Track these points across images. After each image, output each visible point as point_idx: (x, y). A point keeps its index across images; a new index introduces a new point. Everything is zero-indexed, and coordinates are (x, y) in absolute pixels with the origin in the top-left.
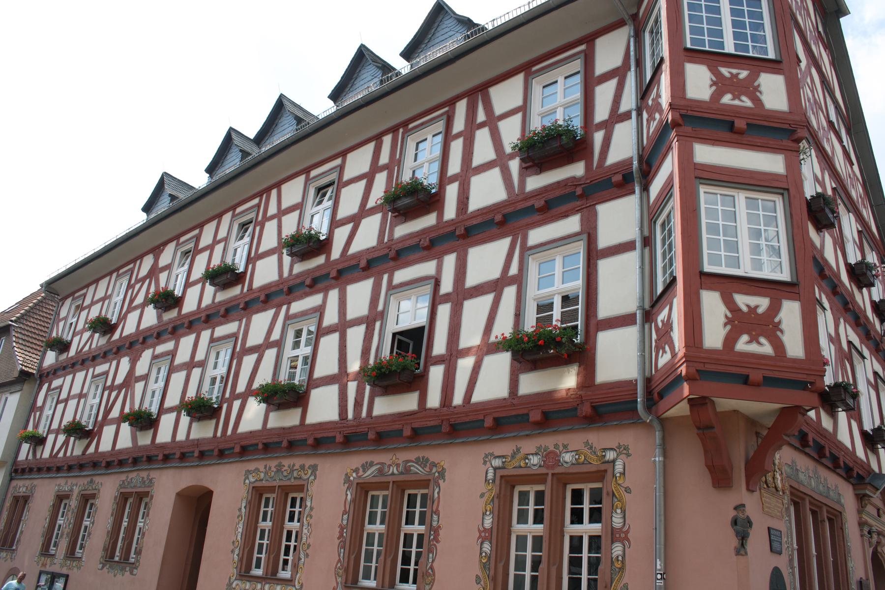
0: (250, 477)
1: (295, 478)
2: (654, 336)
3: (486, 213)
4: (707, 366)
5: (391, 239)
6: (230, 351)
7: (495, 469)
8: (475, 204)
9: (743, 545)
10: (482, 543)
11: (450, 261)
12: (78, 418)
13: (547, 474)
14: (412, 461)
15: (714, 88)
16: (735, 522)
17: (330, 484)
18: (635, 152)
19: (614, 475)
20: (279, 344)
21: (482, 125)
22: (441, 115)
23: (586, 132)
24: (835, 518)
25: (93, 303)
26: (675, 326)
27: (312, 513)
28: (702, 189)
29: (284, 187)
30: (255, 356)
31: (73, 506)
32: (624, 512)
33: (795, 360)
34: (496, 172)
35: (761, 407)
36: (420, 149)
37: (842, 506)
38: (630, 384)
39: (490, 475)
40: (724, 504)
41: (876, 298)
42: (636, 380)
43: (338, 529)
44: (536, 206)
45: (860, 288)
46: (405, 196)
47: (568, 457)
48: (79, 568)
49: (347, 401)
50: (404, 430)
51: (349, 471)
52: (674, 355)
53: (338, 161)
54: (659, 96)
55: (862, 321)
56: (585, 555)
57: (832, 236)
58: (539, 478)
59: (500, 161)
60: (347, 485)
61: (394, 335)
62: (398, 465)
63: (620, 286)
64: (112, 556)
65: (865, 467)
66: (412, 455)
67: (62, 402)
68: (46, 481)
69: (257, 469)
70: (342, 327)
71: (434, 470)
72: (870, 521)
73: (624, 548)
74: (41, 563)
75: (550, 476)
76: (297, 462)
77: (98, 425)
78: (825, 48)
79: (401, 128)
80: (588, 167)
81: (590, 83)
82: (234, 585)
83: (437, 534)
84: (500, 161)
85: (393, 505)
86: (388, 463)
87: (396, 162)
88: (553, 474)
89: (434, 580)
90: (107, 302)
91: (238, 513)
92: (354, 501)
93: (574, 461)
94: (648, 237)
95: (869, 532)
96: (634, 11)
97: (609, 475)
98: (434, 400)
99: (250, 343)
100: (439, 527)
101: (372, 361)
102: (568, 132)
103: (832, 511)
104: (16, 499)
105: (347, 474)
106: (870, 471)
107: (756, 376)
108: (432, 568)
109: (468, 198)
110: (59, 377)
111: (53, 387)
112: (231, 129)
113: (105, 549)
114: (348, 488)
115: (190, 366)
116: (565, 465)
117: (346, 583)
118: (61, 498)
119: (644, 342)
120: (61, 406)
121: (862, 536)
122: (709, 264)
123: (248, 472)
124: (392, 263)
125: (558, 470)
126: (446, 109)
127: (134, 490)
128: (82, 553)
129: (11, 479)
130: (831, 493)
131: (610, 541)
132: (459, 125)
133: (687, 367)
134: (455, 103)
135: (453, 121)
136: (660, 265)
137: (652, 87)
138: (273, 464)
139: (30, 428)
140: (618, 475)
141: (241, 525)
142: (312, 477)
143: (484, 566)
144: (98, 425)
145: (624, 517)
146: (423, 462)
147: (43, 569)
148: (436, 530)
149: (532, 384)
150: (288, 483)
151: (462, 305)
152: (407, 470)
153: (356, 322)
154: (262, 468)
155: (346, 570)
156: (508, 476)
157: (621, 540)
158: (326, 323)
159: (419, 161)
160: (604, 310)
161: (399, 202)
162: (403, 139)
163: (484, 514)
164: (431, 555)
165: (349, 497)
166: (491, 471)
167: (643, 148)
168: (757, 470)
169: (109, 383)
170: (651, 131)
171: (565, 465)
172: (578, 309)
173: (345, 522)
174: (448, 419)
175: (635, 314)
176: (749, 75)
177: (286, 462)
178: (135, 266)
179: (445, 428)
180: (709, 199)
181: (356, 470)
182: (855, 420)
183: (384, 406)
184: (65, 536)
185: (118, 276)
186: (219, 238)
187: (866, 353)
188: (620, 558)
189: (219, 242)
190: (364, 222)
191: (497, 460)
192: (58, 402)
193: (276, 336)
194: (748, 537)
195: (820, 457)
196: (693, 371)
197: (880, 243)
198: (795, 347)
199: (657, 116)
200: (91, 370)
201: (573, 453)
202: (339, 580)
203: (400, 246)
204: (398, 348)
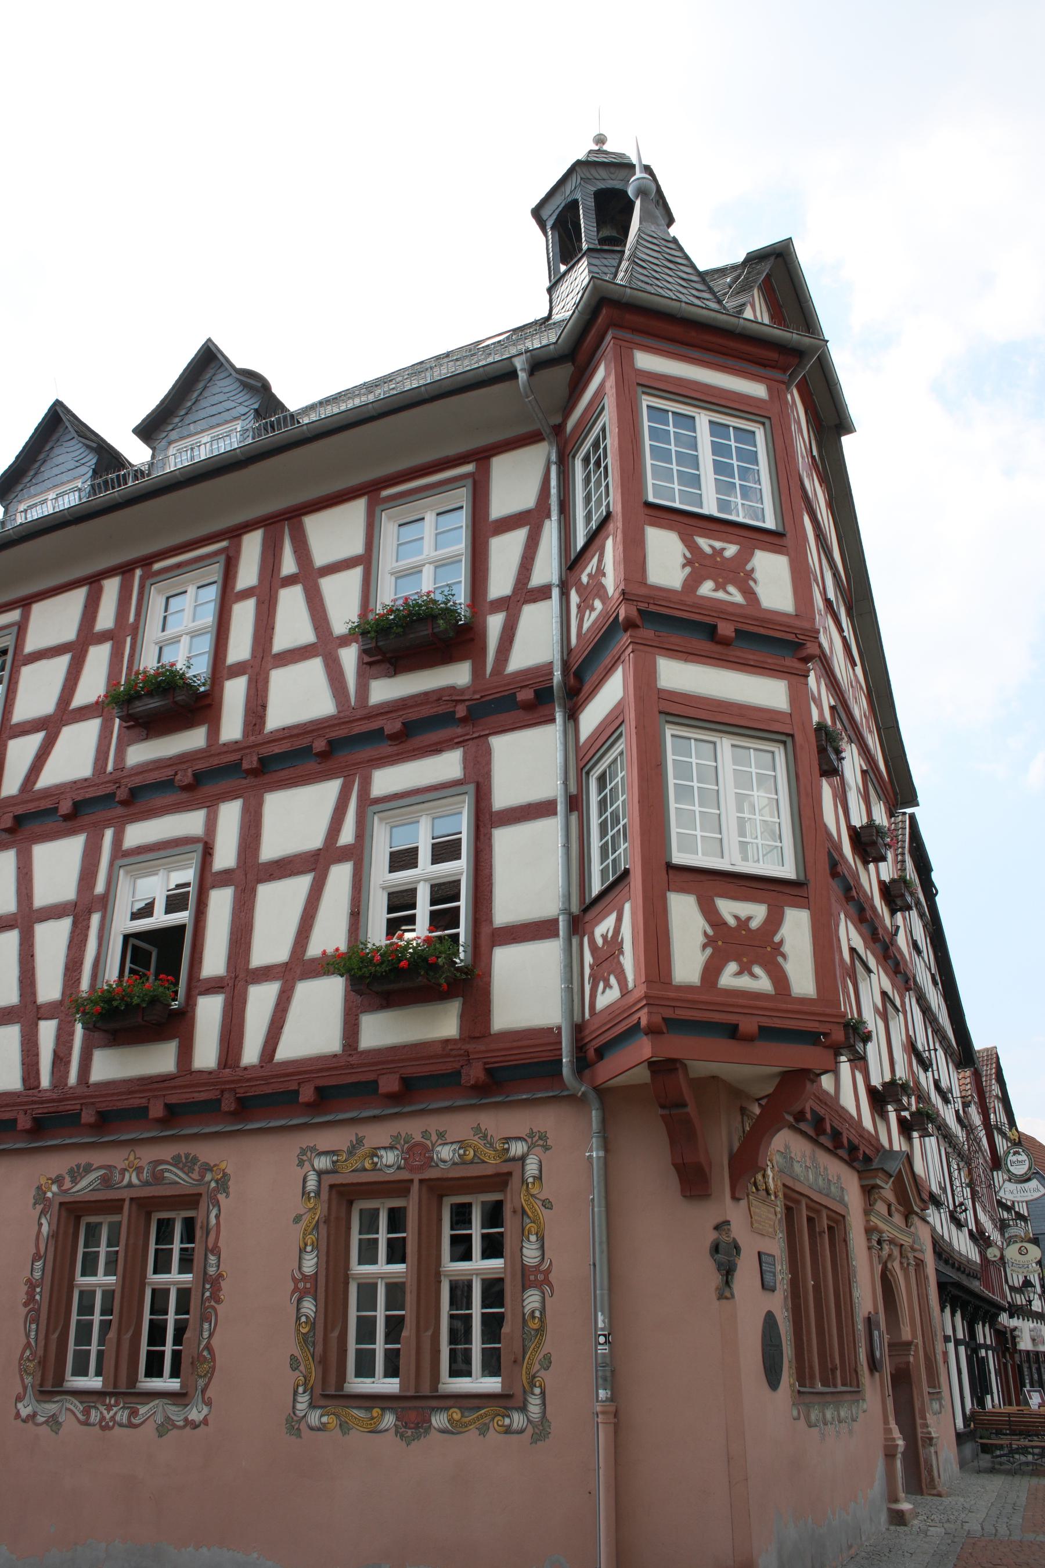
2: (588, 958)
3: (297, 735)
4: (678, 1012)
5: (120, 766)
7: (320, 1174)
8: (276, 719)
9: (728, 1283)
10: (300, 1301)
11: (230, 813)
13: (412, 1181)
14: (168, 1163)
15: (688, 570)
16: (716, 1248)
19: (524, 1181)
21: (290, 581)
23: (474, 614)
24: (838, 1222)
26: (628, 947)
28: (669, 731)
32: (541, 1239)
33: (803, 1001)
34: (315, 666)
35: (753, 1069)
36: (171, 610)
37: (846, 1206)
38: (548, 1036)
39: (312, 1184)
40: (700, 1220)
41: (885, 877)
42: (559, 1028)
45: (866, 863)
46: (150, 694)
49: (37, 1055)
50: (151, 1106)
51: (43, 1181)
52: (625, 992)
53: (15, 615)
54: (600, 572)
55: (869, 913)
56: (477, 1311)
57: (831, 785)
58: (401, 1188)
59: (324, 646)
60: (39, 1208)
61: (127, 938)
62: (139, 1170)
63: (529, 873)
65: (874, 1142)
66: (166, 1152)
71: (208, 1177)
72: (881, 1225)
73: (544, 1298)
75: (416, 1184)
78: (822, 481)
79: (140, 569)
80: (477, 671)
81: (482, 531)
84: (324, 646)
87: (126, 633)
88: (421, 1181)
92: (54, 1235)
93: (457, 1159)
94: (576, 796)
95: (879, 1242)
96: (557, 420)
97: (516, 1179)
98: (206, 1054)
100: (220, 1276)
101: (85, 985)
102: (449, 612)
103: (834, 1215)
105: (39, 1188)
106: (879, 1148)
107: (748, 1025)
108: (208, 1347)
109: (264, 707)
114: (43, 1213)
117: (41, 1385)
121: (870, 1248)
122: (679, 851)
124: (120, 810)
125: (431, 1174)
126: (224, 544)
130: (833, 1189)
131: (520, 1287)
132: (248, 575)
133: (650, 1013)
134: (240, 535)
135: (236, 566)
136: (595, 844)
137: (588, 555)
140: (530, 1180)
143: (305, 1340)
146: (187, 1164)
148: (216, 1282)
149: (380, 1031)
151: (253, 892)
152: (158, 1178)
153: (53, 912)
155: (43, 1363)
157: (538, 1285)
159: (170, 631)
160: (503, 914)
161: (138, 703)
162: (142, 587)
163: (302, 1251)
164: (206, 1326)
165: (45, 1229)
166: (312, 1178)
167: (570, 651)
168: (745, 1165)
170: (586, 625)
172: (458, 908)
173: (37, 1275)
174: (233, 1089)
176: (739, 552)
179: (228, 1104)
180: (684, 752)
181: (58, 1180)
182: (861, 1072)
183: (109, 1066)
187: (872, 962)
188: (537, 1314)
190: (68, 733)
191: (323, 1159)
194: (735, 1270)
195: (836, 1148)
196: (657, 1019)
197: (889, 787)
198: (803, 980)
199: (598, 604)
201: (454, 1146)
202: (28, 1380)
203: (137, 781)
204: (131, 962)
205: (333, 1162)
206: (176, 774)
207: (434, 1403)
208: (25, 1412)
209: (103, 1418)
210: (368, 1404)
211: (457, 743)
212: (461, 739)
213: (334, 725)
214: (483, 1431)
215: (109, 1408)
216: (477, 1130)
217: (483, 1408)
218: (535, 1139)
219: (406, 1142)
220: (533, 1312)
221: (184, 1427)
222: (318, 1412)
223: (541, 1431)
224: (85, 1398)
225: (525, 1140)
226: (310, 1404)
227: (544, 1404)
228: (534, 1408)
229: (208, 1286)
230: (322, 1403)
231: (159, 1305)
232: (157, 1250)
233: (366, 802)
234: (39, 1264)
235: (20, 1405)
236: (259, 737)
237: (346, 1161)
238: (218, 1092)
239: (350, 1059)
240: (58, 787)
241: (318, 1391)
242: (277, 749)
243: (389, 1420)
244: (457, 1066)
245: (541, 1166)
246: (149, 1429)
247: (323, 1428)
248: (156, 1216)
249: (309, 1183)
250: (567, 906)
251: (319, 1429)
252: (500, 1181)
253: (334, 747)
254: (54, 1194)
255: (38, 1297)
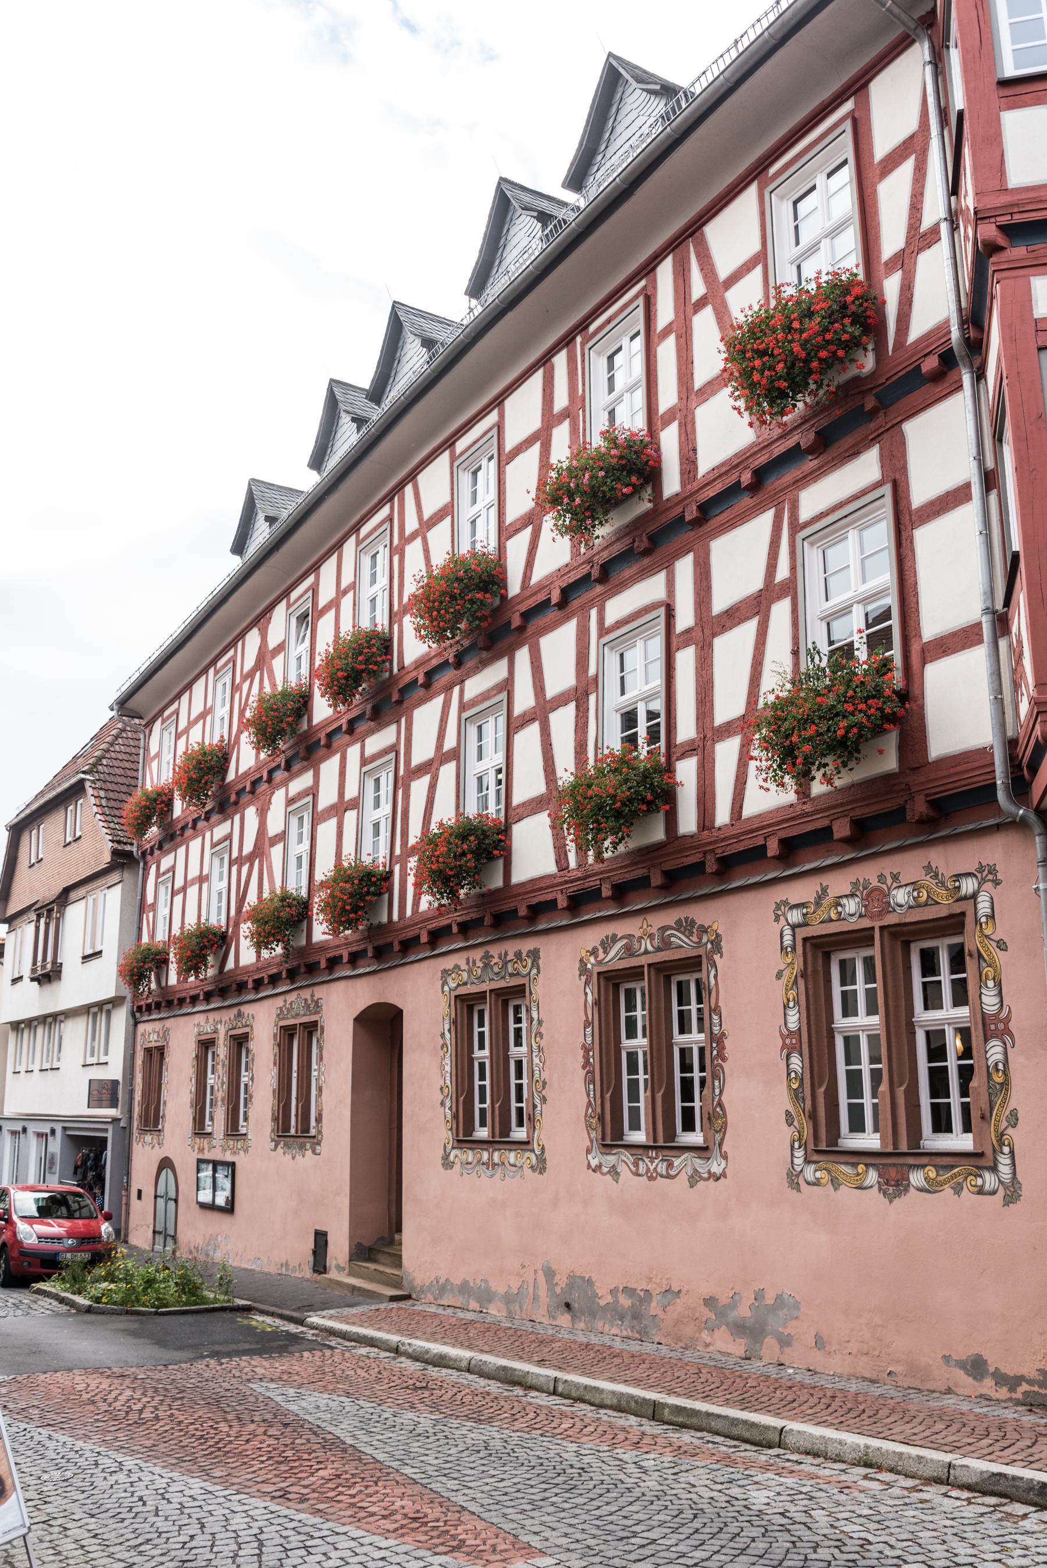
0: (449, 980)
1: (511, 975)
3: (726, 473)
6: (391, 775)
7: (794, 927)
11: (685, 567)
12: (203, 920)
13: (873, 928)
14: (673, 928)
17: (561, 975)
18: (953, 307)
19: (977, 921)
20: (455, 755)
22: (636, 297)
25: (191, 724)
27: (542, 1030)
29: (421, 478)
30: (426, 780)
31: (222, 1057)
32: (999, 985)
36: (800, 215)
38: (984, 752)
39: (788, 939)
43: (581, 1053)
44: (804, 444)
47: (901, 896)
48: (246, 1151)
51: (584, 954)
53: (493, 417)
60: (584, 978)
62: (651, 936)
64: (286, 1128)
66: (669, 918)
67: (179, 892)
68: (182, 1021)
69: (457, 967)
70: (542, 712)
71: (705, 939)
73: (1006, 1049)
74: (196, 1146)
76: (511, 948)
77: (231, 923)
82: (452, 1158)
83: (721, 1048)
85: (653, 1006)
86: (638, 933)
88: (882, 928)
89: (726, 1123)
90: (209, 718)
91: (441, 1042)
92: (597, 1003)
97: (969, 921)
98: (688, 822)
99: (417, 760)
100: (723, 1034)
104: (148, 1051)
105: (581, 960)
108: (720, 1104)
110: (168, 852)
111: (162, 870)
112: (332, 381)
113: (275, 1119)
114: (587, 983)
115: (340, 808)
116: (898, 909)
117: (603, 1139)
118: (206, 1045)
119: (999, 675)
120: (179, 899)
123: (446, 973)
124: (599, 589)
125: (891, 919)
126: (643, 283)
127: (297, 1021)
128: (247, 1126)
129: (136, 1023)
138: (477, 955)
139: (145, 939)
140: (983, 920)
141: (447, 1061)
142: (534, 971)
143: (796, 1095)
144: (231, 923)
145: (1000, 994)
146: (687, 926)
147: (201, 1156)
150: (502, 984)
152: (666, 944)
153: (561, 701)
154: (464, 966)
155: (601, 1119)
156: (813, 937)
158: (518, 710)
160: (933, 624)
164: (717, 1083)
165: (590, 998)
166: (788, 931)
169: (235, 854)
171: (898, 909)
173: (589, 1040)
174: (713, 850)
175: (980, 624)
177: (495, 950)
178: (236, 651)
181: (594, 952)
184: (219, 1103)
185: (216, 672)
186: (343, 586)
188: (1001, 1066)
189: (345, 592)
191: (795, 912)
192: (174, 894)
193: (450, 743)
200: (208, 835)
201: (909, 888)
202: (593, 1135)
205: (804, 915)
206: (634, 541)
207: (911, 1161)
208: (594, 1163)
209: (648, 1170)
210: (854, 1160)
211: (872, 440)
212: (875, 434)
213: (755, 453)
214: (958, 1190)
215: (652, 1161)
216: (928, 868)
217: (957, 1166)
218: (985, 874)
219: (865, 888)
220: (996, 1064)
221: (708, 1179)
222: (813, 1167)
223: (1012, 1193)
224: (634, 1151)
225: (975, 876)
226: (805, 1159)
227: (1013, 1164)
228: (1005, 1170)
229: (714, 1045)
230: (815, 1157)
231: (937, 1052)
232: (924, 984)
233: (796, 527)
234: (589, 1030)
235: (590, 1157)
236: (694, 484)
237: (814, 912)
238: (701, 855)
239: (805, 807)
240: (547, 578)
241: (811, 1146)
242: (711, 492)
243: (872, 1176)
244: (901, 801)
245: (992, 903)
246: (683, 1178)
247: (817, 1183)
248: (512, 1004)
249: (785, 938)
250: (989, 604)
251: (814, 1184)
252: (955, 923)
253: (761, 475)
254: (593, 965)
255: (591, 1060)
